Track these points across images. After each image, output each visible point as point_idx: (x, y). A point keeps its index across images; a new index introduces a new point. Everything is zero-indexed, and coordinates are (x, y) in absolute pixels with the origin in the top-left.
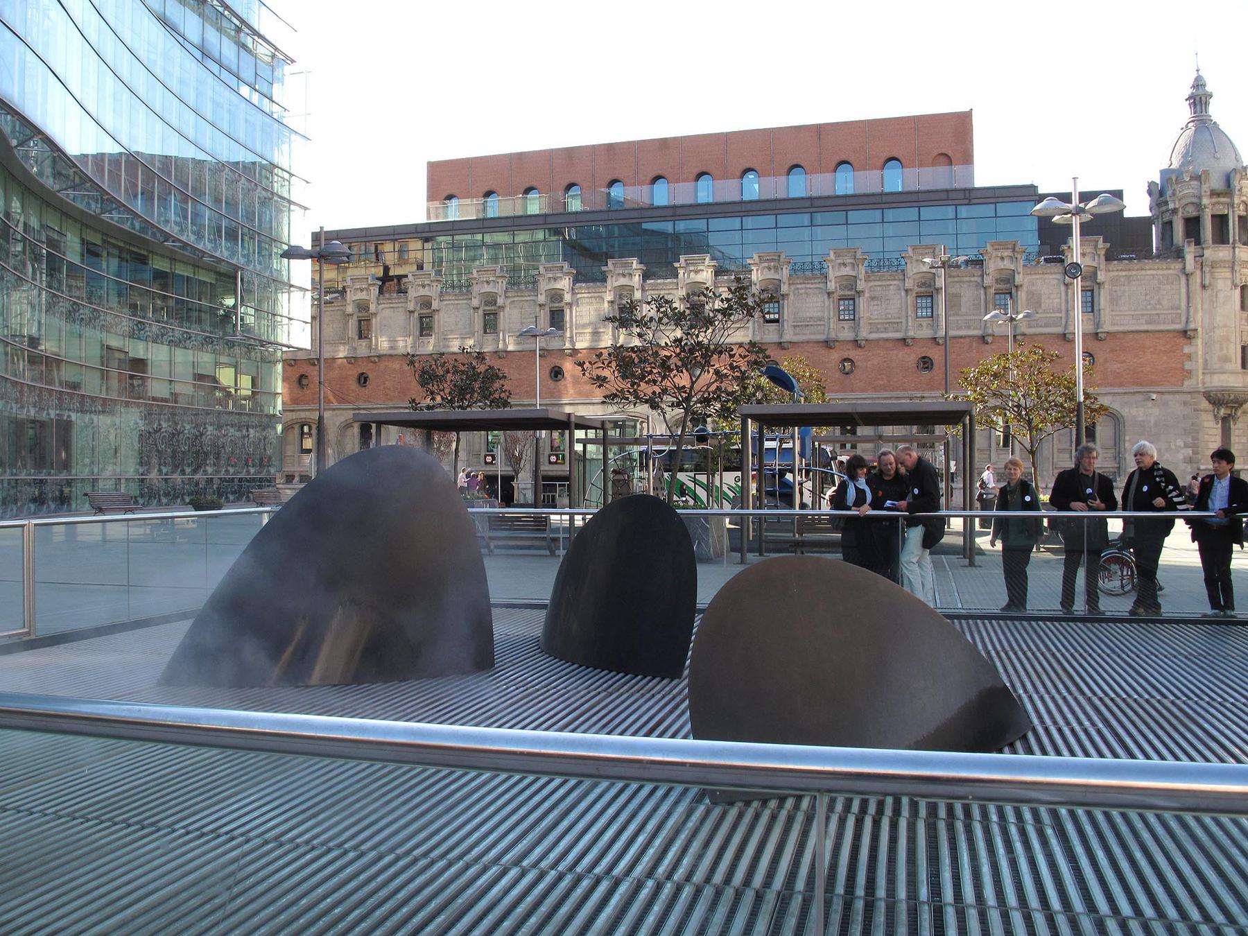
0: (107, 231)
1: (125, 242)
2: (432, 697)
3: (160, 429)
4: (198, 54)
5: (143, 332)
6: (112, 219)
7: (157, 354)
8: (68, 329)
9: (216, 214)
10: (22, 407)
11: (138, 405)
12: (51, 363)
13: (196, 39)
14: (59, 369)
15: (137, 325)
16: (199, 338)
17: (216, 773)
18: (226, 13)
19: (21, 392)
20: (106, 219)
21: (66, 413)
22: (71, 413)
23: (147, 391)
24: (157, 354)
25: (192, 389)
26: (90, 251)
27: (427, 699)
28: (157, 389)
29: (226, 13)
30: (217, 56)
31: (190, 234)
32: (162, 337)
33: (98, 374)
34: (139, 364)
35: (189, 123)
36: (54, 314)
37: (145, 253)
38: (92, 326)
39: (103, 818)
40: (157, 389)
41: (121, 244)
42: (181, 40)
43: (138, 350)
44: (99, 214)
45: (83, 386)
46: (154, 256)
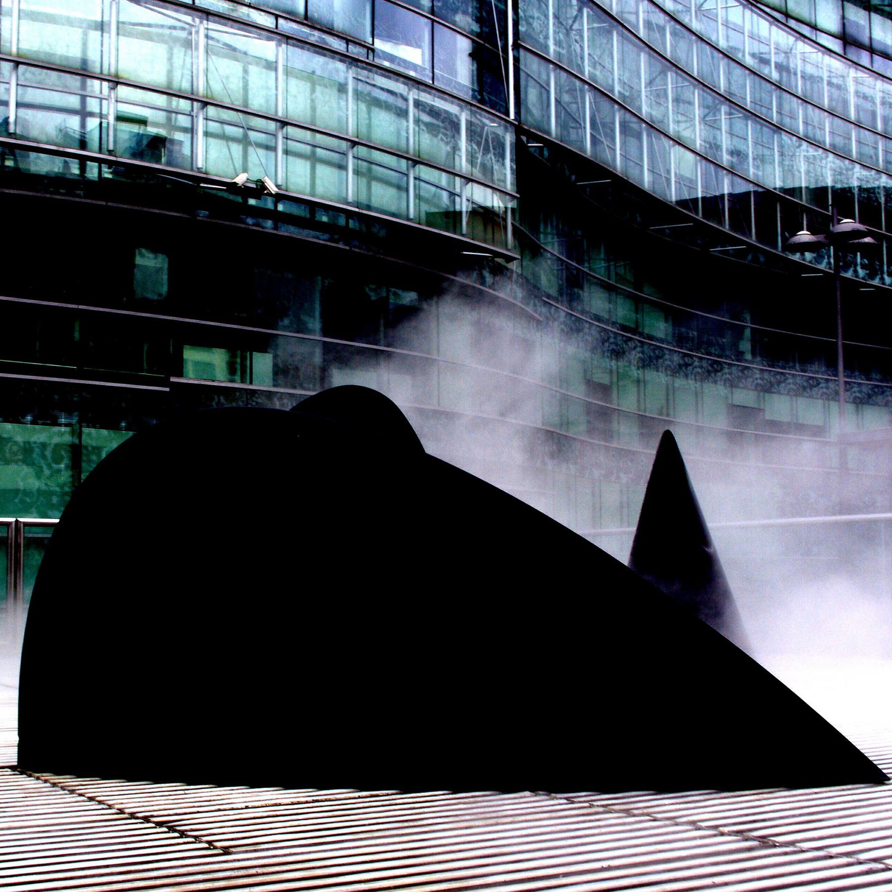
4: (835, 45)
30: (866, 41)
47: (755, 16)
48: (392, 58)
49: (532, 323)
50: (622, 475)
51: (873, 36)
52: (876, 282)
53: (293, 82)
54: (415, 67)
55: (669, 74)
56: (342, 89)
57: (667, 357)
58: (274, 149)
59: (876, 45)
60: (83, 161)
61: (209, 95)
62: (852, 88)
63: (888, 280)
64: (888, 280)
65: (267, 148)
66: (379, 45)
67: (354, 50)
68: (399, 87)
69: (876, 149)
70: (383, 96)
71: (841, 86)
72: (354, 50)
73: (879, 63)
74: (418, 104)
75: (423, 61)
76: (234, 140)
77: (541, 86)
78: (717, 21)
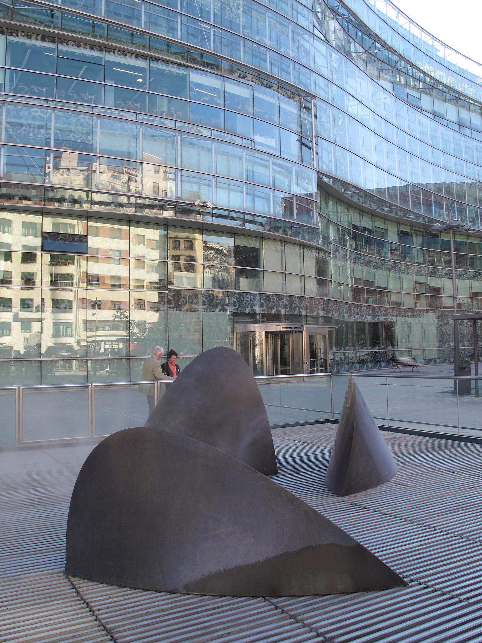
0: (411, 224)
1: (423, 229)
2: (477, 499)
3: (448, 323)
4: (456, 127)
5: (397, 268)
6: (411, 218)
7: (447, 285)
8: (366, 271)
9: (451, 200)
10: (351, 315)
11: (434, 311)
12: (384, 293)
13: (455, 119)
14: (387, 296)
15: (419, 268)
16: (472, 274)
17: (476, 510)
18: (471, 102)
19: (349, 307)
20: (378, 211)
21: (390, 318)
22: (393, 318)
23: (442, 303)
24: (447, 285)
25: (469, 301)
26: (402, 234)
27: (368, 518)
28: (447, 302)
29: (471, 102)
30: (469, 125)
31: (468, 222)
32: (408, 270)
33: (412, 297)
34: (437, 290)
35: (452, 163)
36: (370, 266)
37: (437, 233)
38: (393, 271)
39: (425, 524)
40: (447, 302)
41: (422, 230)
42: (420, 111)
43: (434, 283)
44: (403, 217)
45: (402, 304)
46: (442, 234)
47: (421, 117)
48: (262, 145)
49: (313, 250)
50: (367, 316)
51: (472, 121)
52: (475, 228)
53: (219, 158)
54: (272, 148)
55: (384, 143)
56: (241, 158)
57: (362, 258)
58: (211, 186)
59: (473, 126)
60: (129, 197)
61: (183, 165)
62: (463, 144)
63: (481, 227)
64: (481, 227)
65: (209, 185)
66: (258, 139)
67: (247, 143)
68: (266, 157)
69: (474, 170)
70: (259, 161)
71: (93, 305)
72: (247, 143)
73: (475, 134)
74: (273, 163)
75: (276, 146)
76: (194, 183)
77: (328, 152)
78: (404, 118)
